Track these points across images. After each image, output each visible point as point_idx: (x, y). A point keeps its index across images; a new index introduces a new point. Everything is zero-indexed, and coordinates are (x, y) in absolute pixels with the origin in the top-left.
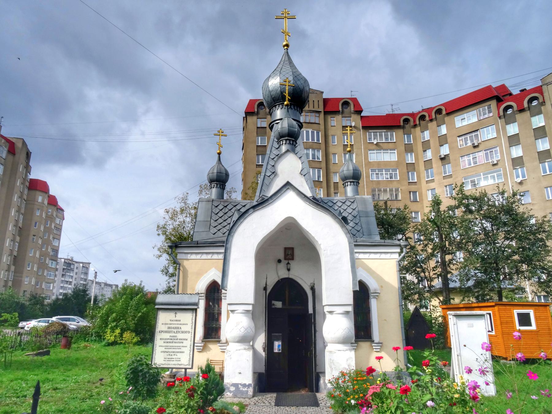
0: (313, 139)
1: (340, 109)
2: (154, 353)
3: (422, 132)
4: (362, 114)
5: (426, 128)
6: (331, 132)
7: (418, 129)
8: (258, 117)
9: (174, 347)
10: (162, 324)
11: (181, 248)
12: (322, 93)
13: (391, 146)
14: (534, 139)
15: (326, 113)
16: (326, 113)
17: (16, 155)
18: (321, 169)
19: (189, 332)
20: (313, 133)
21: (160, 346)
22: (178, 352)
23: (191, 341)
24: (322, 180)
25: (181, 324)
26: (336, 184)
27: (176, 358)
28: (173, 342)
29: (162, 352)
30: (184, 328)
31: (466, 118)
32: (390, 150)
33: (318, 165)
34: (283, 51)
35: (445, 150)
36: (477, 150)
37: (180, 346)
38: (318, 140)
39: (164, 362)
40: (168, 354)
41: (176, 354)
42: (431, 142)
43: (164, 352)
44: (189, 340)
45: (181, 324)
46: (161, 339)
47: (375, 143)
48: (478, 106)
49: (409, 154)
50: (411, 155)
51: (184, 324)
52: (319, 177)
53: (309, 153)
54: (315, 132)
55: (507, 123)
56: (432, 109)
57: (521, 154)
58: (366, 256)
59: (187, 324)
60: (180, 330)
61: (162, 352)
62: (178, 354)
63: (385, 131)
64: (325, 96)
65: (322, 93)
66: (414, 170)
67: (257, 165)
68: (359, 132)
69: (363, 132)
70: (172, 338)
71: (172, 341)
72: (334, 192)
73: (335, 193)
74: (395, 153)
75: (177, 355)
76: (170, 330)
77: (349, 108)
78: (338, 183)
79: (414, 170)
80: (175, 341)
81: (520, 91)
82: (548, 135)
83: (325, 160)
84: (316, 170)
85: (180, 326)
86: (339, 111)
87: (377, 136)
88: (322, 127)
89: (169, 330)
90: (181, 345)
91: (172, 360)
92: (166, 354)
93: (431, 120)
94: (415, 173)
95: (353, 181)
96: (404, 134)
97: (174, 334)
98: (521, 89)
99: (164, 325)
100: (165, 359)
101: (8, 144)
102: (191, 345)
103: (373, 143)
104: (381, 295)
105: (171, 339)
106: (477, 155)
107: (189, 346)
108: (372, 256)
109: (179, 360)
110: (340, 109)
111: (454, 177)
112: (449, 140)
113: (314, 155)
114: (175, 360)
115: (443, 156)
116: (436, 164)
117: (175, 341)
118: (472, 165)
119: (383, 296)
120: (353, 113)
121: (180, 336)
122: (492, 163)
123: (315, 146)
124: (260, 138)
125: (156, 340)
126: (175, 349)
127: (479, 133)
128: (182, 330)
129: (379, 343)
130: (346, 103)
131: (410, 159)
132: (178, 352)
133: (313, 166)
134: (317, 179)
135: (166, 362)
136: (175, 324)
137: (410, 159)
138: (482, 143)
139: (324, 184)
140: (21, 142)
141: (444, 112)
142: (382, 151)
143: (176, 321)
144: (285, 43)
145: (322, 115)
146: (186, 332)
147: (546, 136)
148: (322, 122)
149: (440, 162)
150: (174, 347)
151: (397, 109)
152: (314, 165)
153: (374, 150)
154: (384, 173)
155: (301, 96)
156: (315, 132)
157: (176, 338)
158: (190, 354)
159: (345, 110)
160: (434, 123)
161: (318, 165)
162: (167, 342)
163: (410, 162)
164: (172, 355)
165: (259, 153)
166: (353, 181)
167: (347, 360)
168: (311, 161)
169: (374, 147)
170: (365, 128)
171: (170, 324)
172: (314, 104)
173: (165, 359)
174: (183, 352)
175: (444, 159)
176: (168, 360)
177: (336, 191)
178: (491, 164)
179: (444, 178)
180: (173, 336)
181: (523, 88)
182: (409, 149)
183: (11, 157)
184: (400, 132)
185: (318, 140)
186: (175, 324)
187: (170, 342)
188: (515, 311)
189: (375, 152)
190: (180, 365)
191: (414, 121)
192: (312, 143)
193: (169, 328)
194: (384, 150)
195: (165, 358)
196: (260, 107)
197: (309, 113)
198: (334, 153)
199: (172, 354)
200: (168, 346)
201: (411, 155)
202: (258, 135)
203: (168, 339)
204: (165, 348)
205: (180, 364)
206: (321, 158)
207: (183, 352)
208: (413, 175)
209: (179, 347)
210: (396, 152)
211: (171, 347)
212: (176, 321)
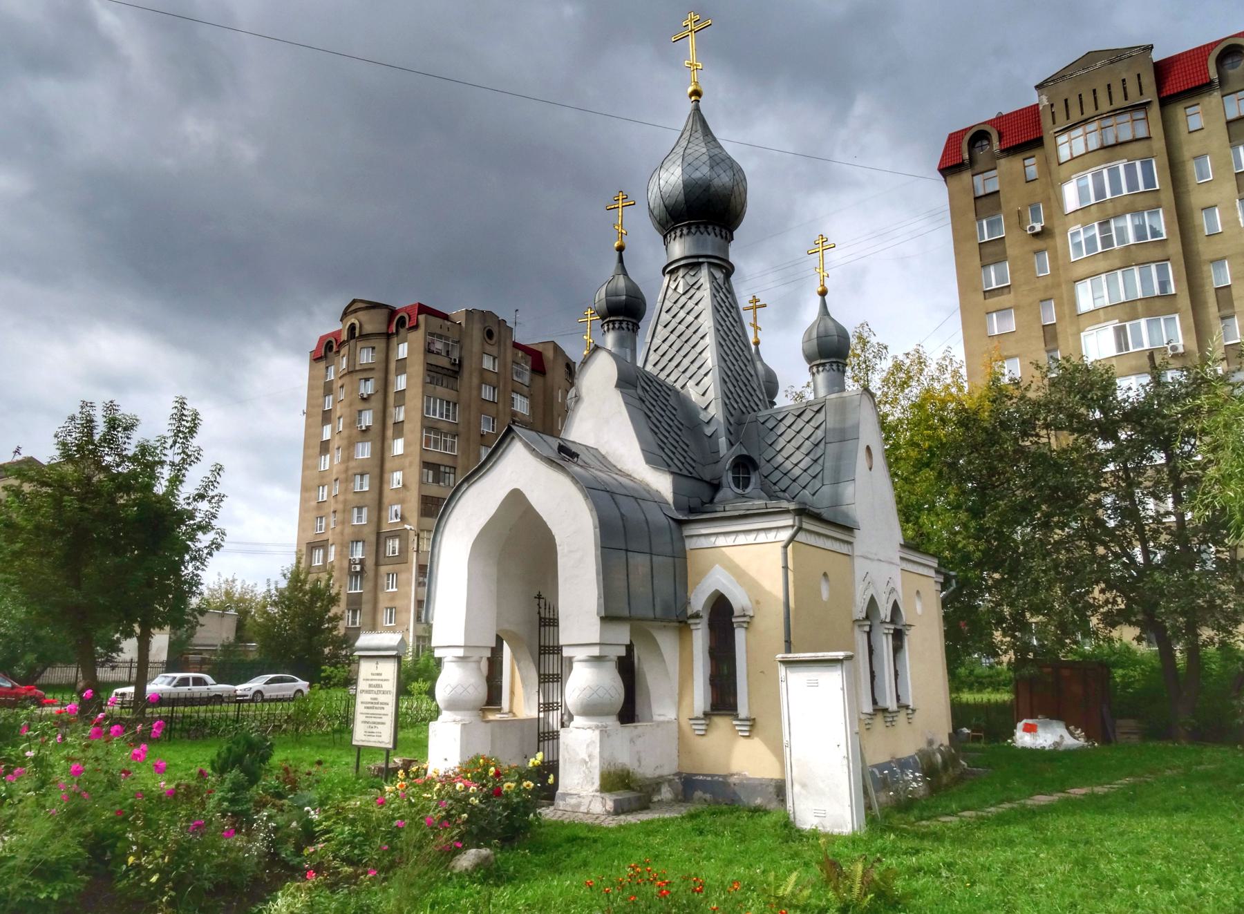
1: (1213, 74)
8: (975, 172)
12: (1150, 48)
15: (1166, 102)
16: (1166, 102)
17: (547, 375)
18: (1168, 260)
20: (1130, 170)
22: (379, 723)
24: (1174, 292)
26: (1225, 290)
33: (1157, 253)
38: (1149, 181)
39: (364, 738)
43: (365, 722)
44: (390, 704)
53: (1126, 227)
54: (1138, 164)
58: (730, 540)
64: (1157, 56)
65: (1150, 48)
67: (985, 292)
72: (1218, 314)
73: (1223, 318)
78: (1229, 286)
83: (1178, 232)
84: (1153, 267)
88: (1159, 144)
90: (382, 712)
95: (823, 361)
97: (375, 696)
101: (529, 358)
104: (756, 620)
108: (742, 539)
119: (760, 623)
121: (382, 698)
124: (985, 222)
129: (747, 720)
132: (379, 723)
133: (1141, 260)
134: (1157, 292)
139: (1184, 302)
140: (551, 347)
144: (690, 89)
145: (1155, 111)
148: (1157, 132)
159: (1230, 72)
165: (986, 261)
166: (823, 361)
167: (588, 746)
172: (1125, 89)
174: (383, 723)
177: (1226, 312)
180: (376, 699)
183: (539, 380)
187: (372, 708)
192: (1132, 198)
193: (370, 686)
196: (979, 144)
198: (1203, 206)
202: (979, 217)
206: (1164, 231)
207: (383, 723)
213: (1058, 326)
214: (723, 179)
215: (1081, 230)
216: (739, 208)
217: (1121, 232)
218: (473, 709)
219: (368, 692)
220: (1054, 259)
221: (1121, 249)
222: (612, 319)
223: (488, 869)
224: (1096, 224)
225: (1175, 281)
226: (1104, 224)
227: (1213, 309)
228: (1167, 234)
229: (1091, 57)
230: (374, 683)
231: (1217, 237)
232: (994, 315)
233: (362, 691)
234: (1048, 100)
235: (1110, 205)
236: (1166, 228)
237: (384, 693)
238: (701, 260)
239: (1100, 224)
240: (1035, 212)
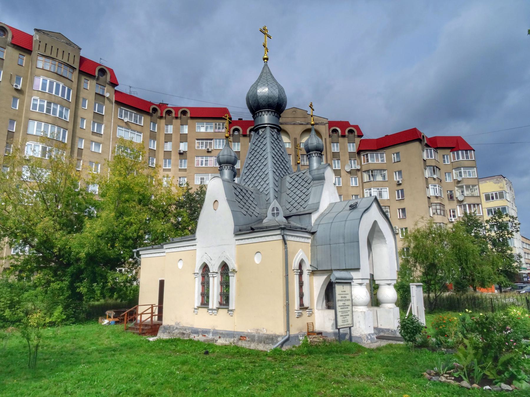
0: (63, 95)
3: (166, 125)
5: (171, 123)
6: (83, 94)
7: (163, 121)
11: (287, 231)
12: (80, 49)
13: (138, 128)
20: (64, 88)
32: (137, 132)
33: (64, 125)
34: (263, 64)
35: (183, 147)
36: (209, 154)
39: (342, 324)
42: (173, 136)
47: (126, 121)
49: (152, 141)
50: (154, 142)
52: (64, 137)
54: (67, 88)
56: (179, 108)
63: (135, 112)
66: (154, 156)
68: (111, 105)
74: (141, 136)
77: (104, 77)
79: (154, 156)
84: (62, 130)
85: (345, 295)
86: (95, 76)
87: (128, 116)
93: (177, 118)
94: (155, 159)
96: (151, 122)
97: (343, 302)
98: (239, 118)
106: (209, 159)
110: (97, 74)
111: (188, 171)
112: (188, 140)
113: (61, 113)
115: (182, 152)
116: (175, 157)
118: (204, 166)
120: (108, 84)
123: (65, 103)
127: (213, 142)
130: (103, 71)
131: (153, 145)
135: (346, 323)
137: (153, 145)
138: (214, 150)
141: (189, 115)
142: (130, 131)
144: (265, 57)
145: (77, 72)
149: (178, 155)
152: (60, 123)
153: (122, 127)
155: (258, 103)
156: (67, 88)
159: (100, 77)
160: (179, 121)
161: (64, 125)
163: (152, 148)
169: (124, 124)
175: (182, 154)
177: (79, 158)
179: (180, 170)
180: (344, 304)
181: (241, 118)
182: (153, 136)
184: (148, 118)
185: (69, 98)
189: (124, 129)
191: (162, 113)
193: (342, 297)
194: (132, 130)
197: (63, 65)
201: (154, 142)
208: (153, 160)
210: (142, 135)
213: (15, 134)
215: (39, 100)
217: (55, 111)
218: (366, 305)
219: (341, 300)
220: (21, 104)
221: (53, 117)
224: (46, 101)
225: (68, 139)
226: (49, 103)
227: (75, 155)
228: (69, 120)
229: (60, 36)
230: (343, 296)
231: (46, 122)
233: (339, 300)
234: (39, 38)
235: (53, 97)
236: (70, 118)
238: (266, 125)
239: (48, 102)
240: (18, 79)
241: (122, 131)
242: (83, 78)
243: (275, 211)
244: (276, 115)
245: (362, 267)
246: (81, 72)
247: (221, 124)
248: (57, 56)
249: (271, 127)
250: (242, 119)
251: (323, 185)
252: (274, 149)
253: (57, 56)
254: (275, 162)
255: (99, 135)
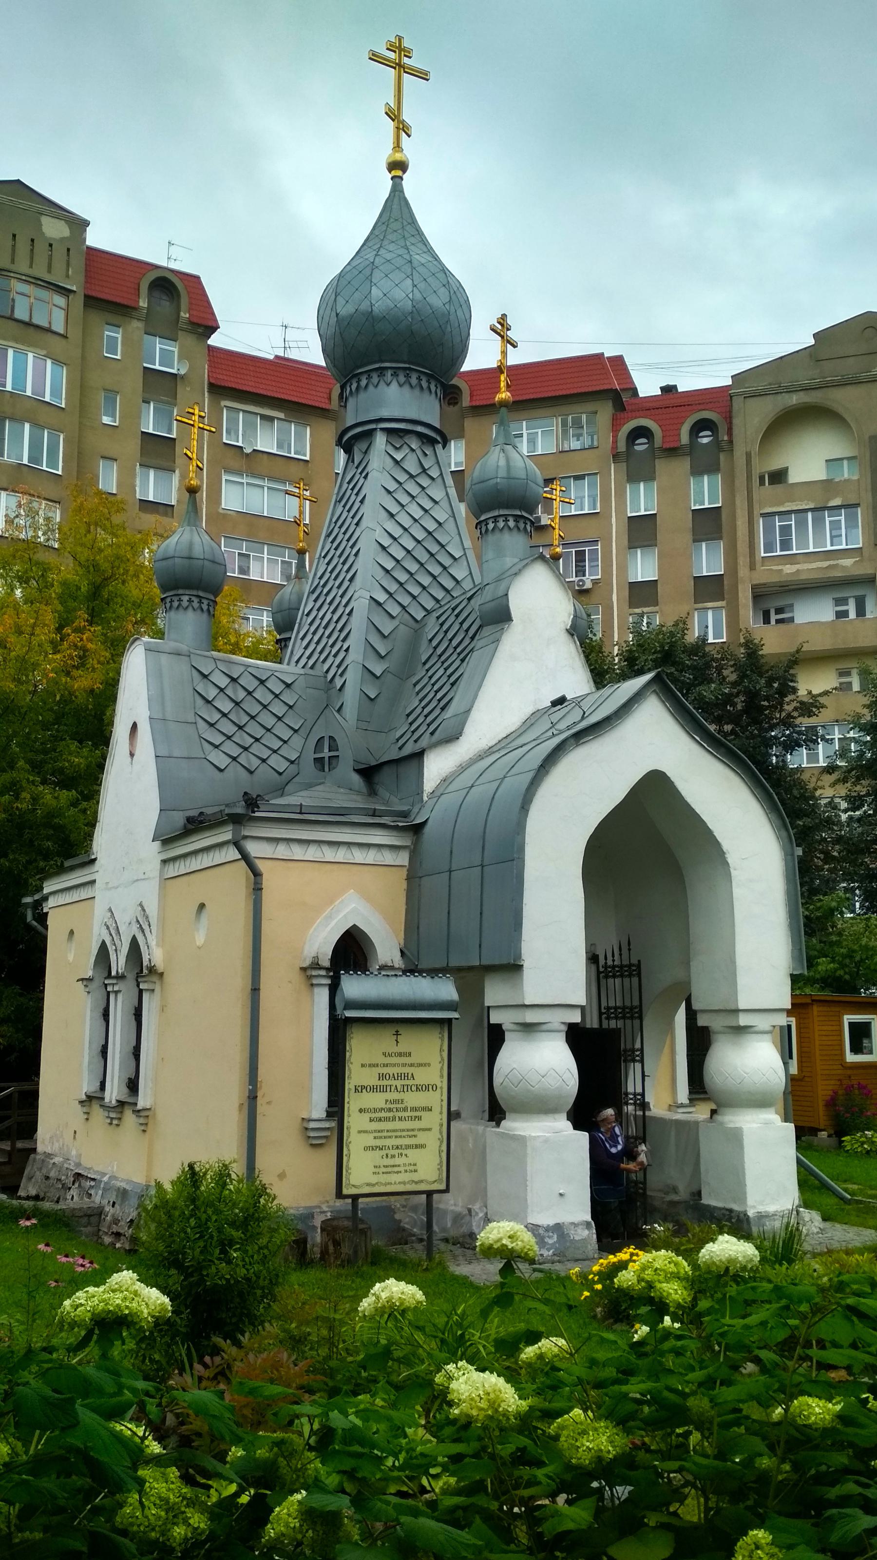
2: (345, 1152)
4: (212, 342)
9: (399, 1134)
10: (363, 1066)
14: (689, 537)
19: (434, 1088)
21: (360, 1132)
23: (441, 1113)
25: (412, 1065)
27: (405, 1165)
28: (394, 1119)
29: (366, 1149)
30: (422, 1077)
31: (525, 436)
37: (413, 1130)
39: (374, 1179)
40: (384, 1152)
41: (404, 1152)
43: (373, 1148)
44: (436, 1109)
45: (412, 1065)
46: (361, 1111)
48: (564, 409)
51: (420, 1065)
55: (633, 477)
57: (651, 575)
59: (429, 1065)
60: (410, 1082)
61: (366, 1149)
62: (409, 1152)
63: (282, 415)
69: (209, 400)
70: (392, 1106)
71: (391, 1114)
75: (406, 1155)
76: (385, 1082)
80: (400, 1114)
81: (662, 389)
82: (725, 534)
89: (381, 1083)
90: (416, 1124)
91: (396, 1169)
92: (379, 1153)
99: (367, 1069)
100: (377, 1170)
102: (442, 1125)
103: (241, 447)
105: (390, 1110)
107: (436, 1129)
109: (412, 1168)
110: (143, 303)
114: (402, 1169)
117: (400, 1114)
121: (413, 1099)
122: (579, 585)
125: (349, 1116)
126: (400, 1137)
128: (418, 1081)
136: (398, 1065)
143: (400, 1055)
146: (427, 1088)
147: (720, 538)
150: (399, 1134)
151: (300, 344)
154: (266, 556)
157: (403, 1106)
158: (440, 1152)
162: (380, 1120)
164: (393, 1156)
168: (25, 469)
170: (217, 390)
171: (386, 1065)
173: (377, 1170)
176: (385, 1170)
178: (577, 588)
180: (396, 1101)
186: (398, 1065)
187: (387, 1119)
188: (846, 1017)
190: (416, 1183)
193: (382, 1077)
195: (375, 1167)
199: (396, 1152)
200: (382, 1131)
203: (382, 1110)
204: (375, 1138)
205: (416, 1180)
209: (412, 1133)
211: (390, 1134)
212: (400, 1055)
214: (438, 300)
216: (457, 340)
222: (502, 512)
223: (819, 1515)
232: (810, 515)
237: (418, 1088)
241: (257, 491)
242: (96, 318)
243: (326, 750)
244: (414, 381)
245: (529, 959)
246: (92, 302)
247: (584, 417)
248: (13, 261)
249: (389, 431)
250: (675, 387)
251: (498, 641)
252: (392, 516)
253: (13, 261)
254: (389, 564)
255: (161, 508)
